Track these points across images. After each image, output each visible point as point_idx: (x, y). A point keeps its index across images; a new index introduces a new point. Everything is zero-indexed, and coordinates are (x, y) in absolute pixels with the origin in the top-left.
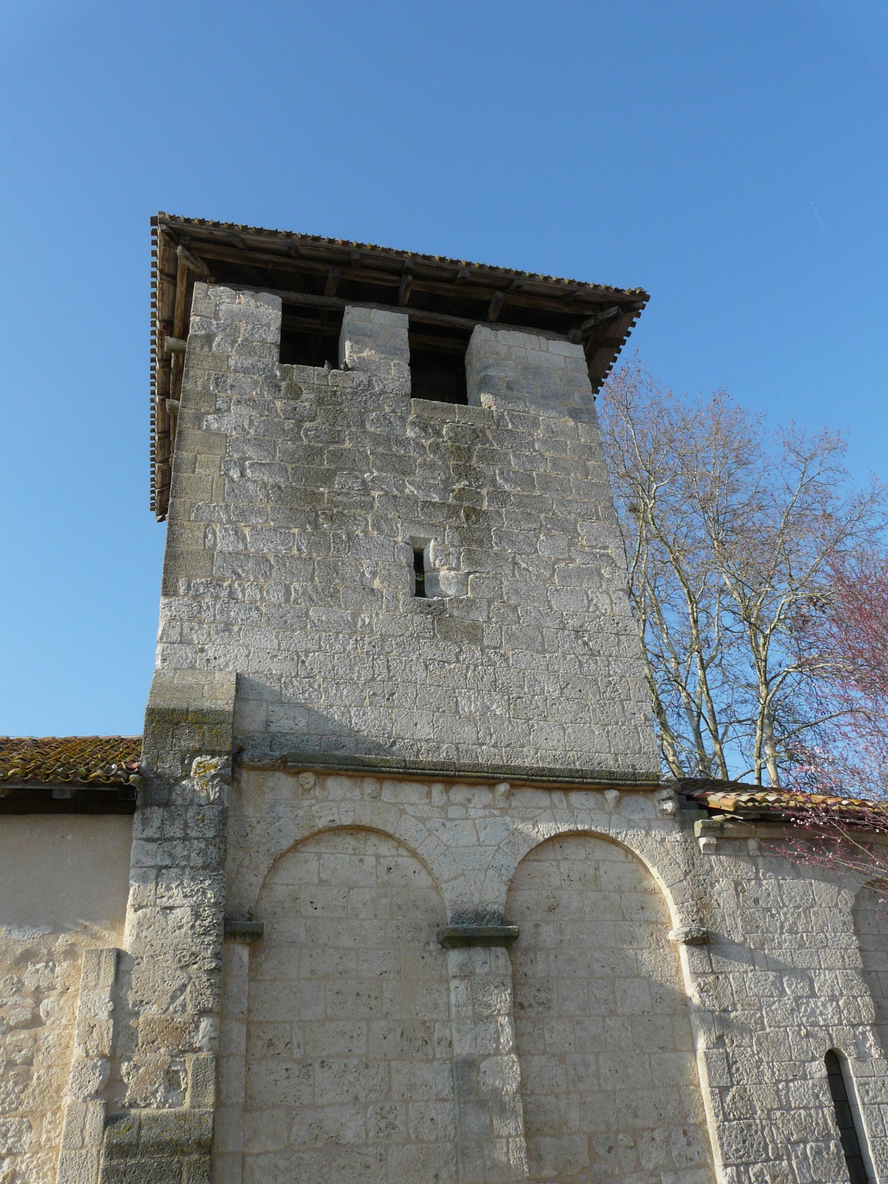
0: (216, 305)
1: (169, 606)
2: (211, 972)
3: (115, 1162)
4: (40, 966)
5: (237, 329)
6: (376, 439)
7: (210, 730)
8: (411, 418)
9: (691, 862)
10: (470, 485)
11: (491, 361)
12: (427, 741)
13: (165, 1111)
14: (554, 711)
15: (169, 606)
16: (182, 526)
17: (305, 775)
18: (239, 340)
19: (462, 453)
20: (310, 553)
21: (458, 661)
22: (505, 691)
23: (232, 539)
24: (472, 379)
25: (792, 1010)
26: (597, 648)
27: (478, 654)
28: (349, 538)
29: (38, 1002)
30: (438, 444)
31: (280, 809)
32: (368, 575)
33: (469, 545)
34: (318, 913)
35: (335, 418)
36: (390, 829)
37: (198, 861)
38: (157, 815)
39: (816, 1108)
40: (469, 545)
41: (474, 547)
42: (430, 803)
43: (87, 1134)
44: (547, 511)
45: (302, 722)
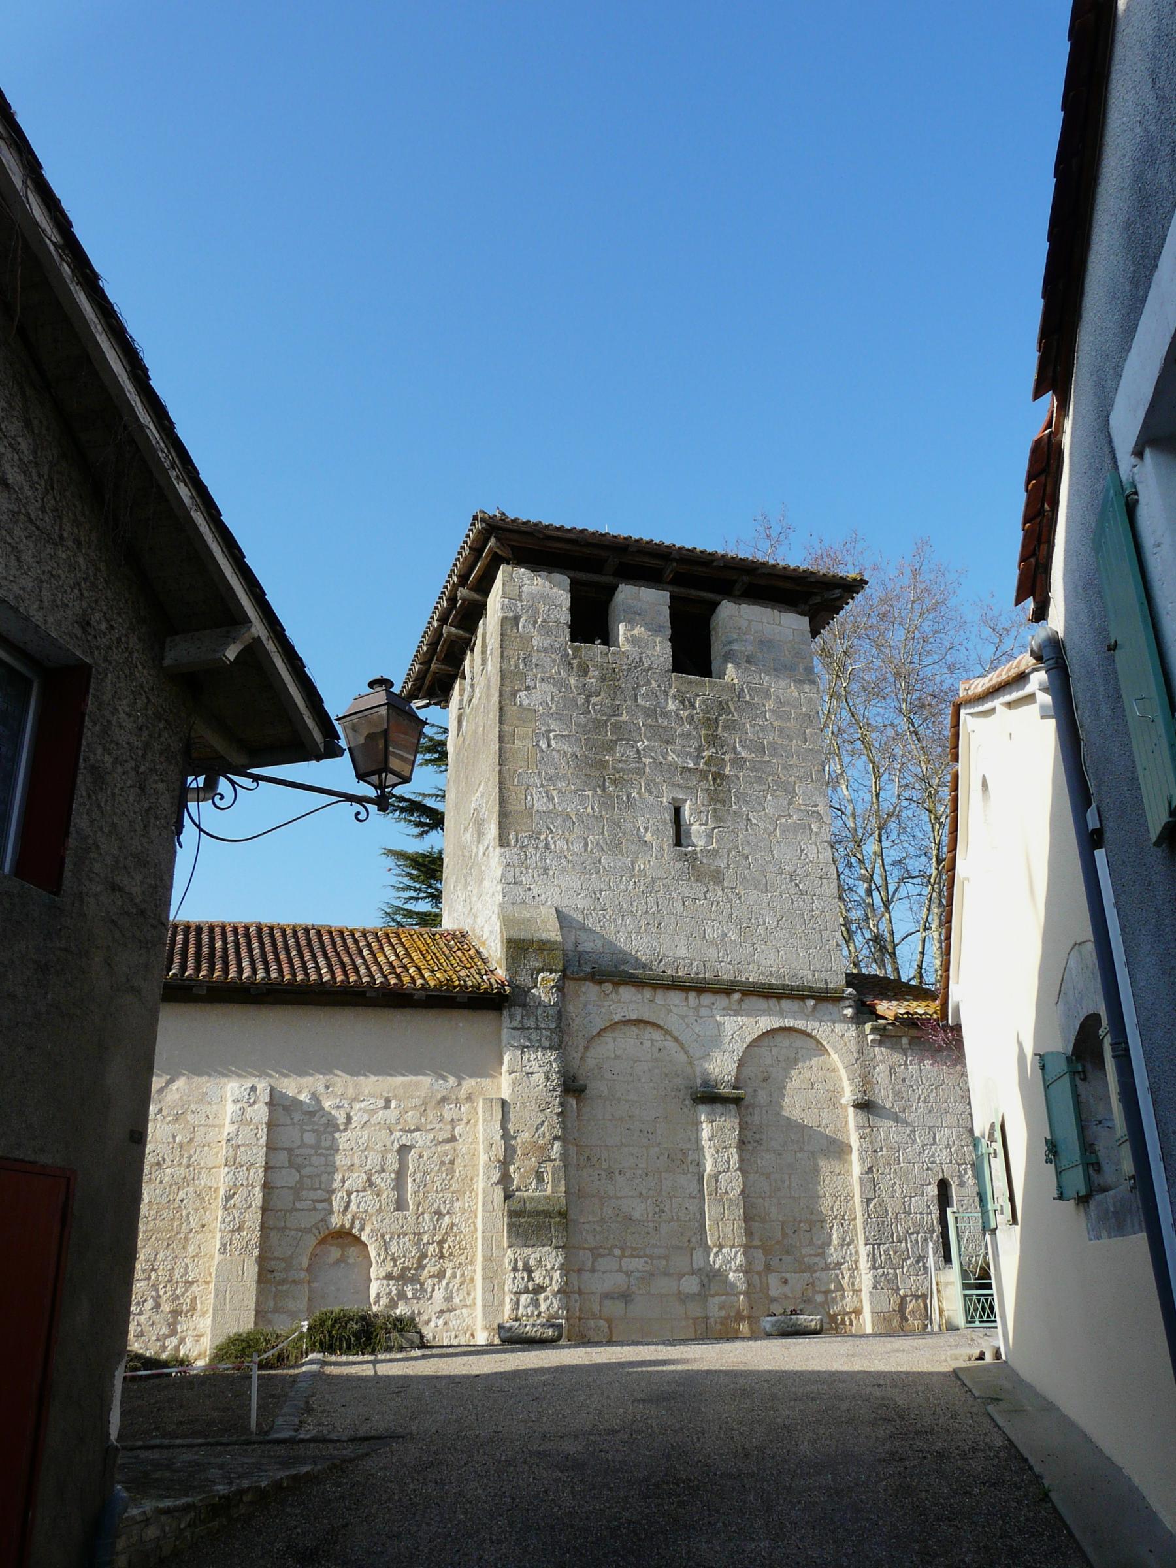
0: (520, 588)
1: (504, 854)
2: (558, 1114)
3: (513, 1220)
4: (453, 1106)
5: (536, 611)
6: (645, 710)
7: (549, 955)
8: (672, 692)
9: (861, 1051)
10: (717, 753)
11: (735, 636)
12: (683, 959)
13: (537, 1194)
14: (772, 938)
15: (504, 854)
16: (509, 790)
17: (606, 984)
18: (539, 620)
19: (711, 723)
20: (600, 812)
21: (706, 899)
22: (738, 922)
23: (544, 800)
24: (717, 650)
25: (920, 1153)
26: (805, 888)
27: (720, 893)
28: (629, 800)
29: (454, 1128)
30: (692, 716)
31: (590, 1007)
32: (642, 830)
33: (715, 804)
34: (615, 1077)
35: (615, 693)
36: (662, 1024)
37: (547, 1044)
38: (518, 1012)
39: (928, 1214)
40: (715, 804)
41: (718, 806)
42: (687, 1005)
43: (495, 1204)
44: (773, 774)
45: (599, 943)
